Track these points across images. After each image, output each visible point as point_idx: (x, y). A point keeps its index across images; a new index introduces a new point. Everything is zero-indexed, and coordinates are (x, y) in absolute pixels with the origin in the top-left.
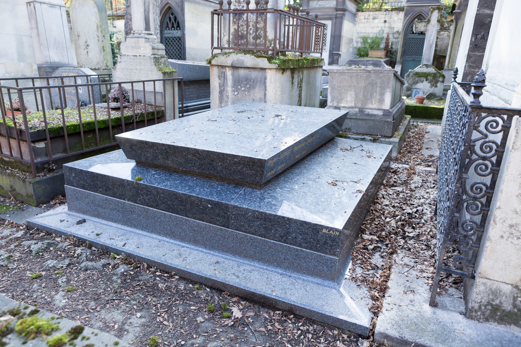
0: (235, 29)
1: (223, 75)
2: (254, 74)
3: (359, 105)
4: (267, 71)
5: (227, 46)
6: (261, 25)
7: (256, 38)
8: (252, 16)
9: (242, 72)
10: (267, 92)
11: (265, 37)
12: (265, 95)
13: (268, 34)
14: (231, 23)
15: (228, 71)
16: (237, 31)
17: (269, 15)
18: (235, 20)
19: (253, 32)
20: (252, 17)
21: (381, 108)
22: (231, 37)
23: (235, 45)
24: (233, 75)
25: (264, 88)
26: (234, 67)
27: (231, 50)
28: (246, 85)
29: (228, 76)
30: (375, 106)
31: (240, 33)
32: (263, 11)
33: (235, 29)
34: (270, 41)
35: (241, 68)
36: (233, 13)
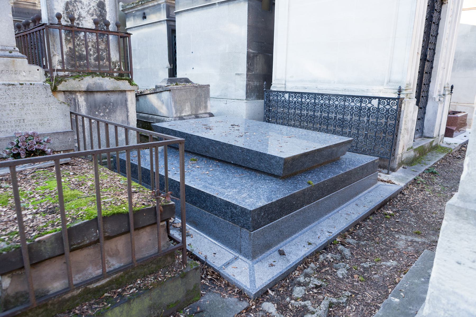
0: (70, 48)
1: (73, 102)
2: (113, 97)
3: (194, 113)
4: (127, 93)
5: (59, 67)
6: (102, 46)
7: (98, 59)
8: (90, 36)
9: (98, 97)
10: (129, 114)
11: (109, 59)
12: (128, 116)
13: (111, 56)
14: (63, 41)
15: (79, 97)
16: (72, 51)
17: (111, 37)
18: (69, 38)
19: (94, 52)
20: (92, 38)
21: (206, 112)
22: (65, 57)
23: (73, 66)
24: (86, 100)
25: (125, 110)
26: (88, 92)
27: (67, 73)
28: (105, 109)
29: (80, 103)
30: (203, 112)
31: (77, 54)
32: (103, 32)
33: (70, 48)
34: (114, 63)
35: (97, 92)
36: (65, 30)
